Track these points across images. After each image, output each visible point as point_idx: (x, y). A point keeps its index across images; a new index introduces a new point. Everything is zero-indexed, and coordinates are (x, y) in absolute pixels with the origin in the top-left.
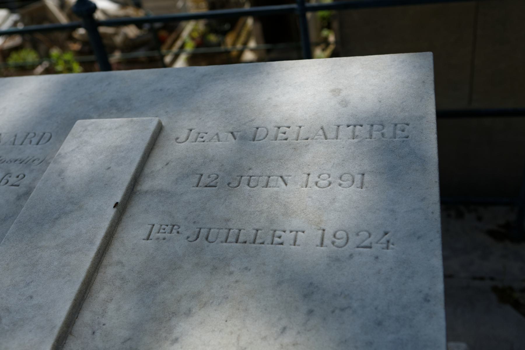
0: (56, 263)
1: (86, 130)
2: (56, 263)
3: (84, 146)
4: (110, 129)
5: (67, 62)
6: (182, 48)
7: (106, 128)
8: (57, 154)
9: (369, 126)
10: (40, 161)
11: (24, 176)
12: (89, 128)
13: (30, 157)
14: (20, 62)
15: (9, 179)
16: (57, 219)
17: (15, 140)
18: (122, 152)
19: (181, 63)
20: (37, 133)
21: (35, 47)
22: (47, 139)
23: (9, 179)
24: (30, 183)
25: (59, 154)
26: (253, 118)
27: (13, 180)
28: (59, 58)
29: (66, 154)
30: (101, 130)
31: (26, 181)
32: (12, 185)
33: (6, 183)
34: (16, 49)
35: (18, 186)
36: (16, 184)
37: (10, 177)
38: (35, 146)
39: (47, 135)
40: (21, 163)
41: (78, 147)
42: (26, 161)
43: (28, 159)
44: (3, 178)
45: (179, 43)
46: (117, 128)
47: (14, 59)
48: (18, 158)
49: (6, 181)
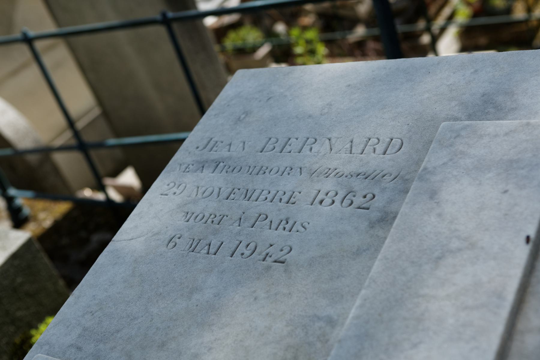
0: (451, 321)
1: (458, 136)
2: (451, 321)
3: (461, 158)
4: (496, 136)
5: (309, 42)
6: (451, 18)
7: (489, 134)
8: (421, 168)
9: (366, 223)
10: (393, 177)
11: (374, 196)
12: (463, 133)
13: (378, 171)
14: (239, 43)
15: (354, 199)
16: (439, 258)
17: (351, 147)
18: (523, 169)
19: (448, 45)
20: (381, 138)
21: (257, 23)
22: (398, 147)
23: (354, 199)
24: (385, 207)
25: (425, 169)
26: (204, 170)
27: (358, 200)
28: (299, 37)
29: (435, 168)
30: (481, 137)
31: (379, 202)
32: (359, 208)
33: (350, 205)
34: (235, 26)
35: (368, 209)
36: (364, 206)
37: (354, 196)
38: (182, 173)
39: (396, 142)
40: (366, 178)
41: (451, 160)
42: (372, 176)
43: (375, 174)
44: (345, 197)
45: (447, 12)
46: (506, 134)
47: (232, 41)
48: (360, 171)
49: (350, 202)
